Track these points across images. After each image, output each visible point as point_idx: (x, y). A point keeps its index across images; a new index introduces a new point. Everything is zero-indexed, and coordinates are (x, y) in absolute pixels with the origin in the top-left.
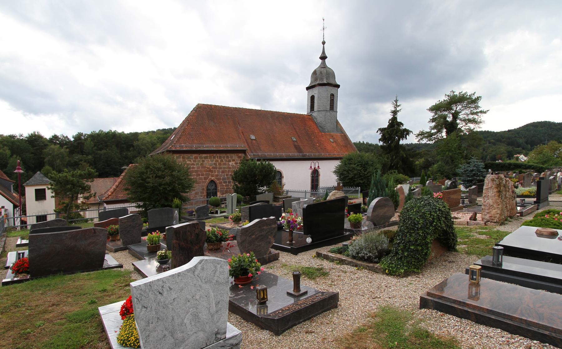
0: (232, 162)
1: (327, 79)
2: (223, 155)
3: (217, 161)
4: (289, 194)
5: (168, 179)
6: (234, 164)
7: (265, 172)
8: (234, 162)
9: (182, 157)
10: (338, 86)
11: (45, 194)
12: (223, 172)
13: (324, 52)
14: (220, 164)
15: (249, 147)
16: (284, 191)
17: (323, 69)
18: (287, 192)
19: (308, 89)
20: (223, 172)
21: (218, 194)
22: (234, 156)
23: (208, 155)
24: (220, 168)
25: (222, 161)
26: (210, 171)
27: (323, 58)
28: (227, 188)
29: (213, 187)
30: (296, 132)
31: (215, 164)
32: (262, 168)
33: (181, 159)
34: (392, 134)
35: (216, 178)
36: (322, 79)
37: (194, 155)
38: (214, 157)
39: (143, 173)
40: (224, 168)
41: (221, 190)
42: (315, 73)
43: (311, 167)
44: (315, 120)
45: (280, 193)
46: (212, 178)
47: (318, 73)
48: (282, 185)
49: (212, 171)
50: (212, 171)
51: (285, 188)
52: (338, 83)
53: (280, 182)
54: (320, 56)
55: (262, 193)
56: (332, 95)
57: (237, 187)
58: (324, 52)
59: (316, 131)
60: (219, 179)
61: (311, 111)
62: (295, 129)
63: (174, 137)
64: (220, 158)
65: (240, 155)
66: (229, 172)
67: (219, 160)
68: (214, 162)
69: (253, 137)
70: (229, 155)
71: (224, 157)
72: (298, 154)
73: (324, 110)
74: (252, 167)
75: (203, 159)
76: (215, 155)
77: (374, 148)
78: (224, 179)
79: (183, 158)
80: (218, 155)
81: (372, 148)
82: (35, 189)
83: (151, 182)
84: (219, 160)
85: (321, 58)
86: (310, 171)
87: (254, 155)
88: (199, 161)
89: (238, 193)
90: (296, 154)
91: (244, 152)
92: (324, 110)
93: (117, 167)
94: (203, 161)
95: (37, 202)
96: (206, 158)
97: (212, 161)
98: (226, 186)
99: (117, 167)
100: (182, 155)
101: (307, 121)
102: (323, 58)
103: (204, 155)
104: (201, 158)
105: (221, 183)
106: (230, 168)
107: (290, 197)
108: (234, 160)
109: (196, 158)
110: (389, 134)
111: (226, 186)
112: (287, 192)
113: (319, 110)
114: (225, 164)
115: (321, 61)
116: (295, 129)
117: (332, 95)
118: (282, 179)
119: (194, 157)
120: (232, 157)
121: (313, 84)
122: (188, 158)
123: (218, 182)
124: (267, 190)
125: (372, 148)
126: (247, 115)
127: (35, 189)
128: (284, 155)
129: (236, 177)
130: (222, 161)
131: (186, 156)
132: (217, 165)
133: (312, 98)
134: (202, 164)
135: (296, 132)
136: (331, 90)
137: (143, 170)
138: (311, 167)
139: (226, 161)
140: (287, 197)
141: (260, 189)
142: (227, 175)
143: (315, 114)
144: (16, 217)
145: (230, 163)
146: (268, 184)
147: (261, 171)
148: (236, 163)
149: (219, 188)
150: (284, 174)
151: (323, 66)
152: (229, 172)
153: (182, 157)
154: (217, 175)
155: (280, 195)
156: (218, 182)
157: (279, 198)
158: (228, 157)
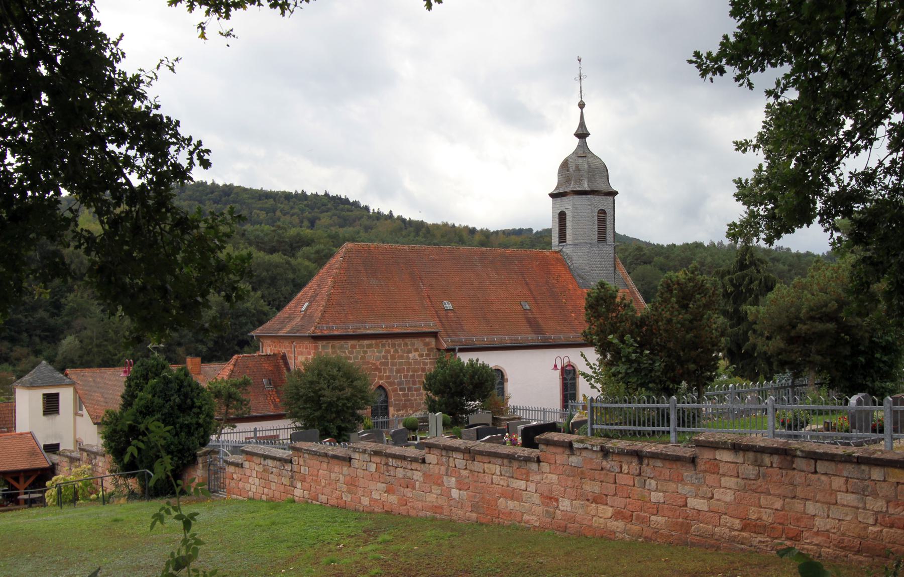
0: (414, 354)
1: (589, 181)
2: (398, 341)
3: (388, 352)
4: (518, 414)
5: (348, 392)
6: (417, 357)
7: (478, 379)
8: (417, 353)
9: (330, 345)
10: (616, 193)
11: (58, 403)
12: (398, 371)
13: (582, 124)
14: (393, 357)
15: (443, 324)
16: (509, 408)
17: (581, 160)
18: (514, 409)
19: (552, 195)
20: (398, 371)
21: (391, 410)
22: (418, 343)
23: (374, 342)
24: (394, 364)
25: (396, 351)
26: (377, 369)
27: (582, 134)
28: (405, 400)
29: (382, 398)
30: (530, 290)
31: (385, 357)
32: (473, 372)
33: (330, 350)
34: (740, 285)
35: (387, 382)
36: (580, 181)
37: (351, 343)
38: (384, 346)
39: (312, 383)
40: (400, 364)
41: (395, 404)
42: (565, 165)
43: (555, 366)
44: (568, 261)
45: (501, 412)
46: (381, 382)
47: (572, 168)
48: (506, 398)
49: (380, 370)
50: (380, 370)
51: (511, 403)
52: (614, 187)
53: (502, 391)
54: (574, 132)
55: (472, 411)
56: (603, 212)
57: (434, 401)
58: (582, 124)
59: (571, 287)
60: (391, 384)
61: (560, 243)
62: (527, 284)
63: (308, 307)
64: (394, 345)
65: (427, 340)
66: (408, 370)
67: (392, 351)
68: (383, 354)
69: (448, 306)
70: (408, 341)
71: (400, 346)
72: (535, 336)
73: (586, 244)
74: (457, 371)
75: (365, 349)
76: (384, 341)
77: (786, 268)
78: (400, 383)
79: (333, 347)
80: (390, 341)
81: (781, 266)
82: (44, 395)
83: (328, 395)
84: (392, 351)
85: (577, 135)
86: (558, 373)
87: (452, 341)
88: (359, 352)
89: (443, 413)
90: (531, 338)
91: (434, 335)
92: (586, 244)
93: (20, 316)
94: (365, 352)
95: (45, 418)
96: (370, 346)
97: (378, 352)
98: (404, 395)
99: (20, 316)
100: (331, 343)
101: (553, 265)
102: (582, 134)
103: (366, 342)
104: (361, 346)
105: (395, 390)
106: (410, 364)
107: (519, 418)
108: (416, 350)
109: (353, 347)
110: (734, 285)
111: (404, 395)
112: (515, 409)
113: (576, 242)
114: (402, 357)
115: (577, 140)
116: (527, 284)
117: (603, 212)
118: (505, 383)
119: (350, 344)
120: (413, 345)
121: (562, 190)
122: (341, 347)
123: (390, 388)
124: (481, 406)
125: (781, 266)
126: (433, 260)
127: (44, 395)
128: (507, 340)
129: (430, 385)
130: (396, 351)
131: (337, 343)
132: (387, 359)
133: (562, 217)
134: (363, 358)
135: (530, 290)
136: (602, 202)
137: (315, 379)
138: (555, 366)
139: (404, 352)
140: (515, 419)
141: (470, 405)
142: (405, 376)
143: (567, 250)
144: (255, 434)
145: (411, 355)
146: (483, 397)
147: (472, 377)
148: (421, 356)
149: (392, 400)
150: (509, 374)
151: (583, 151)
152: (408, 370)
153: (330, 345)
154: (388, 377)
155: (503, 415)
156: (390, 388)
157: (500, 419)
158: (406, 344)
